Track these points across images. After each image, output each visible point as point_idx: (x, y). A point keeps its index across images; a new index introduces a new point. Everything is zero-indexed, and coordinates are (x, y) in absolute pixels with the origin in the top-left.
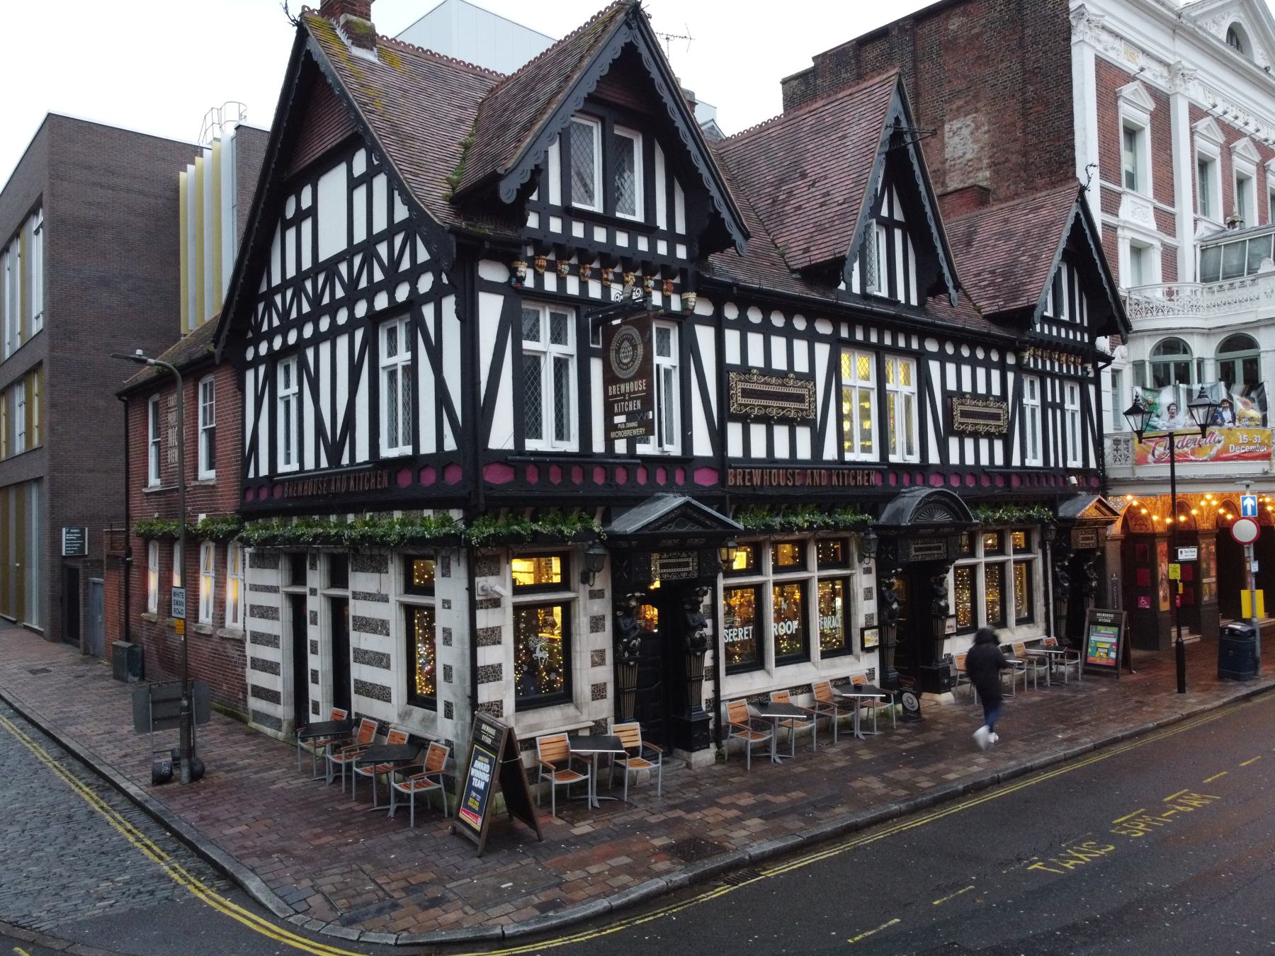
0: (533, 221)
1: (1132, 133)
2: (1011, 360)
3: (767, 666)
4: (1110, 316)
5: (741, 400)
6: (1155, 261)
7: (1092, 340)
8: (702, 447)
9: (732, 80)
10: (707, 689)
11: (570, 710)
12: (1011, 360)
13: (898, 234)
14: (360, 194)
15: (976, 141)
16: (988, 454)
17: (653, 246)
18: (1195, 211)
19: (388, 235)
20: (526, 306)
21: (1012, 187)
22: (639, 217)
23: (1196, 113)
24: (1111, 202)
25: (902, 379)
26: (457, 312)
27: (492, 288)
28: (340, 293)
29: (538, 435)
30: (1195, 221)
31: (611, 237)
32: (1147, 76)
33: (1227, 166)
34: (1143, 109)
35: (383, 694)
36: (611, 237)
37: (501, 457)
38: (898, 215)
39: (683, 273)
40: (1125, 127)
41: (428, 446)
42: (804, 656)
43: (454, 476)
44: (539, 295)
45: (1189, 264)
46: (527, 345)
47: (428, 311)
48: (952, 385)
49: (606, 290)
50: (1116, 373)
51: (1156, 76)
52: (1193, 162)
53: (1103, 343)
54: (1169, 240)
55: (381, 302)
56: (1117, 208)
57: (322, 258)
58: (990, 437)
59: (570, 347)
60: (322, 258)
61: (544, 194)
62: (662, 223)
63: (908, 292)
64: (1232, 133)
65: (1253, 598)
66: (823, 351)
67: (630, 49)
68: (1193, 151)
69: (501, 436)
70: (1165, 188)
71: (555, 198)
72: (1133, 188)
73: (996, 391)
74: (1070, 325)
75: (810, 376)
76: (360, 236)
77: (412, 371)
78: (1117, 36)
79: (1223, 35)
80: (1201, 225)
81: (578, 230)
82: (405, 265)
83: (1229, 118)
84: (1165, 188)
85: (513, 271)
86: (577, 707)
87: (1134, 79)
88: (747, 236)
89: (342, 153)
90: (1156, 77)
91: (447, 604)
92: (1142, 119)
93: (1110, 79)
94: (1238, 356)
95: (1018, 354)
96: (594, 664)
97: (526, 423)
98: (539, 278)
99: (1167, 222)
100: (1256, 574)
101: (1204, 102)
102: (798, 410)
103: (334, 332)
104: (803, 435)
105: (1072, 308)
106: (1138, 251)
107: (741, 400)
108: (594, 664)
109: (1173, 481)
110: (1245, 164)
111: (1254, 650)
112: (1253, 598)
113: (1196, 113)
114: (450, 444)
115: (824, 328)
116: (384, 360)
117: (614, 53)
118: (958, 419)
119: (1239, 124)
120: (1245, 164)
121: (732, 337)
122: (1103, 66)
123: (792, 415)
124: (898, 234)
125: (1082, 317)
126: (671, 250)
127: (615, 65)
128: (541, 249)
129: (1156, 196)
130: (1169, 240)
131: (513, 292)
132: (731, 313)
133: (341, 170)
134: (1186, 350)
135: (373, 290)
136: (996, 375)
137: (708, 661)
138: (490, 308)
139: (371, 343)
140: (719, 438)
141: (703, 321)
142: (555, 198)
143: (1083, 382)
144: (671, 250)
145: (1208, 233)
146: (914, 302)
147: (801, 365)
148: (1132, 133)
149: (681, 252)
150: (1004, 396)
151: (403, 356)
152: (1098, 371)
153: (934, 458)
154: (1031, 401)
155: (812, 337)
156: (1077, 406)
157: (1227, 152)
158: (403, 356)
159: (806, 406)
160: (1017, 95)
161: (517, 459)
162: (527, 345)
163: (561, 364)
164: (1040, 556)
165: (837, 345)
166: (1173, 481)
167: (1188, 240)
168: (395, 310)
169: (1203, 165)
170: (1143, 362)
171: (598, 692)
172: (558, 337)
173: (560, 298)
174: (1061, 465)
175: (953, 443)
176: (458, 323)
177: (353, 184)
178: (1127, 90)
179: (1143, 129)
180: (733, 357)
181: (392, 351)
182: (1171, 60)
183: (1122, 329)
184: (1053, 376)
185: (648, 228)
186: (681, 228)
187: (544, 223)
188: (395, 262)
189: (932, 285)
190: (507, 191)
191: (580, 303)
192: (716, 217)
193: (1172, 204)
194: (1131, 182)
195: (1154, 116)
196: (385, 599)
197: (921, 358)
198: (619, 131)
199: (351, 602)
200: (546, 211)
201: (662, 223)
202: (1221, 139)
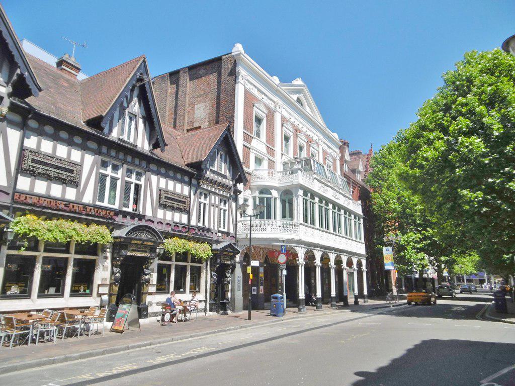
1: (259, 121)
4: (240, 176)
5: (30, 163)
6: (265, 164)
15: (205, 112)
16: (180, 218)
18: (282, 151)
23: (283, 119)
29: (127, 206)
40: (256, 116)
45: (279, 167)
52: (282, 137)
56: (251, 142)
65: (214, 226)
68: (282, 131)
70: (270, 139)
72: (259, 137)
79: (296, 99)
80: (284, 157)
83: (296, 123)
84: (270, 139)
88: (40, 90)
93: (250, 100)
94: (288, 197)
99: (271, 151)
100: (285, 275)
102: (68, 176)
106: (259, 161)
107: (30, 163)
111: (283, 305)
112: (214, 226)
118: (163, 199)
119: (300, 127)
122: (247, 93)
123: (64, 177)
129: (267, 142)
134: (271, 194)
145: (286, 160)
148: (259, 121)
159: (74, 175)
164: (205, 265)
167: (278, 160)
174: (216, 228)
179: (263, 119)
183: (244, 181)
189: (157, 143)
193: (274, 146)
194: (258, 135)
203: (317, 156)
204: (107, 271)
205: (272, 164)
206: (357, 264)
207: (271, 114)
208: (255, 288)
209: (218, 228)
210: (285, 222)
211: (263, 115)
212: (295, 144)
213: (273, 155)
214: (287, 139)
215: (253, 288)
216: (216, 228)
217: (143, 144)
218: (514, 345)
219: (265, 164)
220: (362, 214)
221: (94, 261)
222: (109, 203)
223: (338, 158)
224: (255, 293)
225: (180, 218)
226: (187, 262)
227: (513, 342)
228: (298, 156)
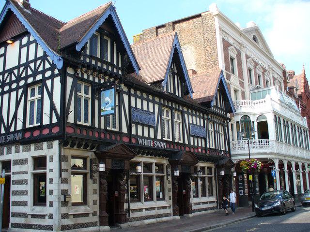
0: (82, 59)
2: (206, 117)
3: (142, 201)
4: (229, 109)
6: (240, 94)
7: (226, 114)
8: (125, 130)
9: (132, 28)
10: (126, 206)
11: (86, 207)
12: (206, 117)
13: (176, 76)
14: (24, 50)
16: (201, 143)
17: (113, 69)
19: (35, 61)
20: (79, 82)
21: (202, 71)
22: (109, 60)
23: (247, 57)
24: (229, 77)
25: (178, 120)
26: (60, 81)
27: (70, 76)
28: (30, 72)
29: (80, 121)
30: (249, 85)
31: (102, 66)
32: (235, 45)
33: (255, 72)
34: (235, 54)
35: (24, 204)
36: (102, 66)
37: (71, 125)
38: (176, 71)
39: (120, 78)
41: (46, 121)
42: (152, 199)
43: (56, 130)
44: (82, 79)
46: (78, 93)
47: (49, 82)
48: (191, 122)
49: (100, 80)
50: (232, 125)
51: (236, 45)
53: (229, 115)
54: (243, 89)
55: (30, 80)
57: (7, 68)
58: (201, 138)
59: (90, 96)
60: (7, 68)
61: (85, 52)
62: (115, 63)
63: (179, 93)
64: (256, 64)
66: (157, 107)
67: (110, 16)
69: (71, 119)
71: (88, 53)
73: (202, 125)
74: (220, 109)
75: (154, 113)
76: (23, 61)
77: (41, 101)
78: (227, 33)
79: (252, 38)
80: (250, 86)
81: (93, 62)
82: (24, 75)
83: (255, 59)
85: (76, 71)
86: (88, 206)
87: (232, 45)
89: (19, 37)
90: (169, 181)
91: (51, 170)
92: (234, 56)
95: (208, 115)
96: (94, 194)
97: (77, 117)
98: (82, 75)
101: (249, 54)
103: (10, 91)
104: (152, 130)
105: (221, 104)
106: (236, 91)
108: (94, 194)
109: (249, 154)
110: (260, 72)
113: (247, 57)
114: (55, 120)
115: (157, 100)
116: (29, 98)
117: (106, 16)
119: (257, 61)
120: (260, 72)
121: (133, 99)
124: (176, 76)
125: (223, 107)
126: (118, 71)
127: (107, 19)
128: (83, 66)
130: (243, 89)
131: (75, 77)
132: (132, 92)
133: (17, 43)
135: (27, 77)
136: (202, 120)
137: (126, 197)
138: (70, 81)
139: (25, 92)
140: (129, 128)
141: (126, 93)
142: (88, 53)
143: (224, 126)
144: (118, 71)
146: (180, 96)
147: (151, 110)
149: (120, 73)
150: (204, 127)
151: (37, 96)
152: (228, 123)
153: (187, 142)
154: (211, 130)
155: (154, 103)
156: (223, 133)
157: (255, 69)
158: (37, 96)
160: (202, 46)
161: (75, 125)
162: (78, 93)
163: (86, 102)
165: (160, 105)
166: (249, 154)
168: (35, 83)
169: (250, 71)
170: (239, 122)
171: (95, 203)
172: (86, 92)
173: (87, 81)
174: (103, 127)
175: (192, 139)
176: (60, 84)
177: (21, 47)
178: (230, 48)
180: (133, 105)
181: (33, 95)
182: (240, 42)
184: (217, 123)
185: (112, 64)
186: (120, 66)
187: (85, 59)
188: (36, 69)
190: (78, 48)
191: (92, 83)
192: (131, 64)
193: (243, 80)
194: (233, 73)
195: (237, 55)
196: (26, 172)
197: (182, 113)
198: (105, 37)
199: (12, 176)
200: (86, 56)
201: (115, 63)
202: (254, 64)
203: (269, 82)
204: (96, 183)
205: (243, 94)
206: (279, 165)
207: (239, 56)
208: (242, 191)
209: (105, 127)
210: (260, 141)
211: (234, 56)
212: (264, 79)
213: (244, 88)
214: (250, 71)
215: (240, 191)
216: (103, 127)
217: (179, 93)
218: (308, 224)
219: (240, 94)
220: (307, 127)
221: (35, 169)
222: (85, 122)
223: (283, 81)
224: (242, 195)
225: (201, 143)
226: (46, 157)
227: (309, 222)
228: (258, 85)
